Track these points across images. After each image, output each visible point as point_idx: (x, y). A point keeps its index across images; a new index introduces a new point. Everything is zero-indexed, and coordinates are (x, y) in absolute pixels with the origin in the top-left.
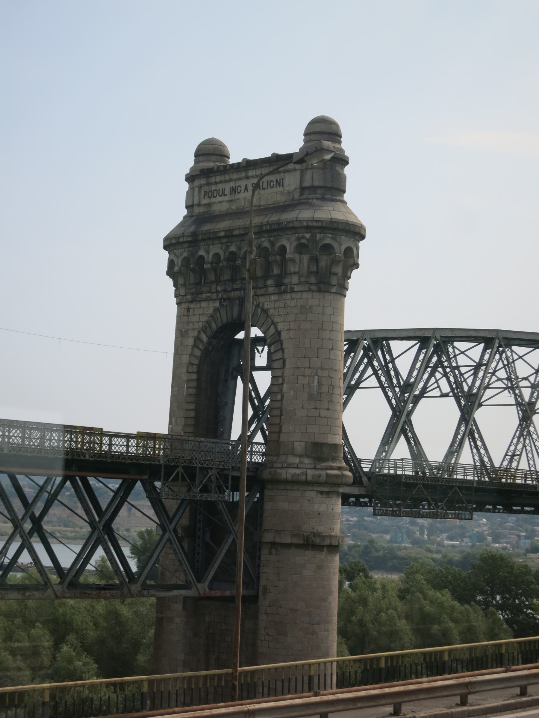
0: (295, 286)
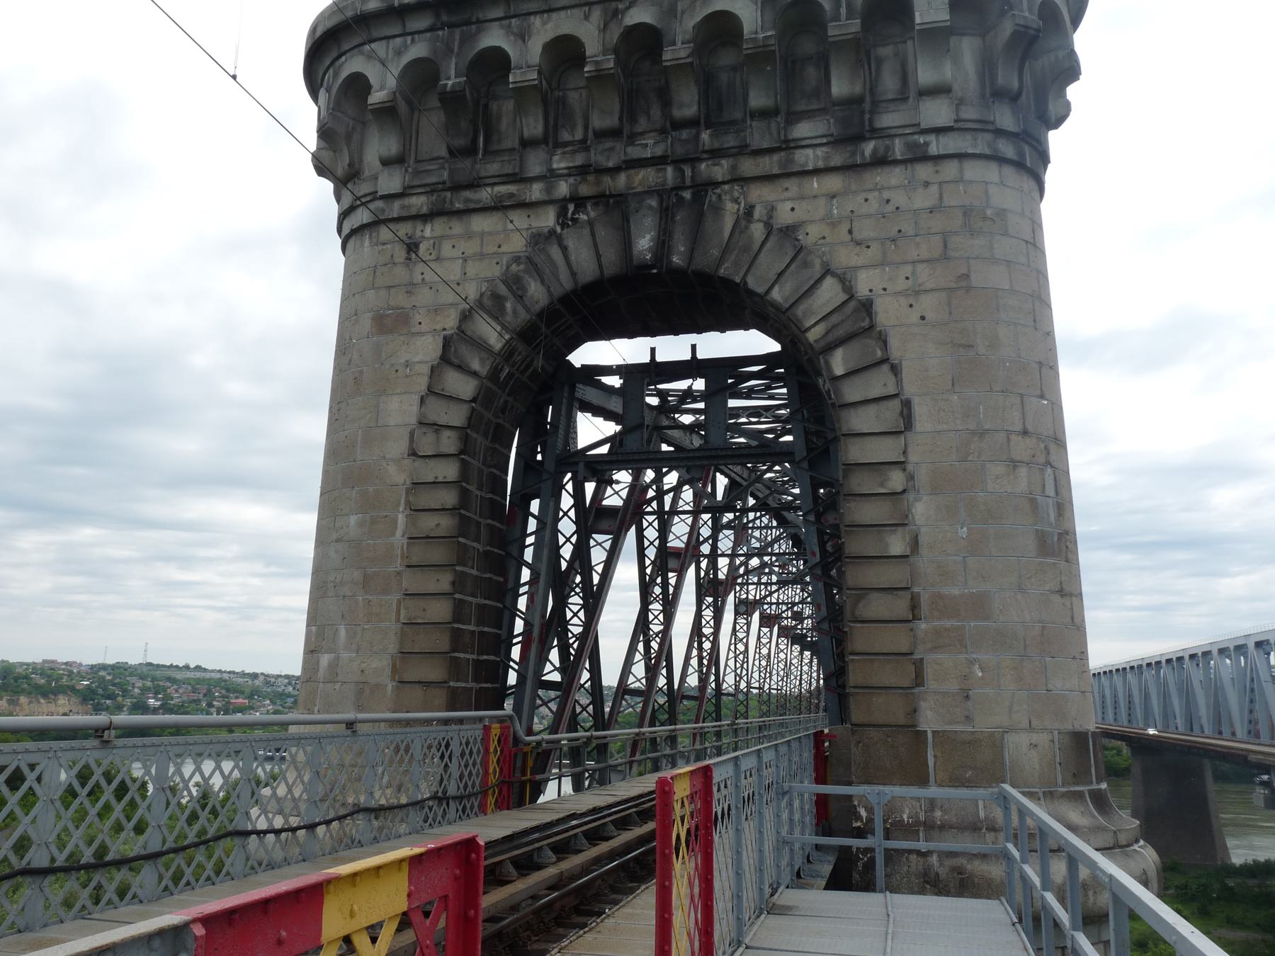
0: (932, 138)
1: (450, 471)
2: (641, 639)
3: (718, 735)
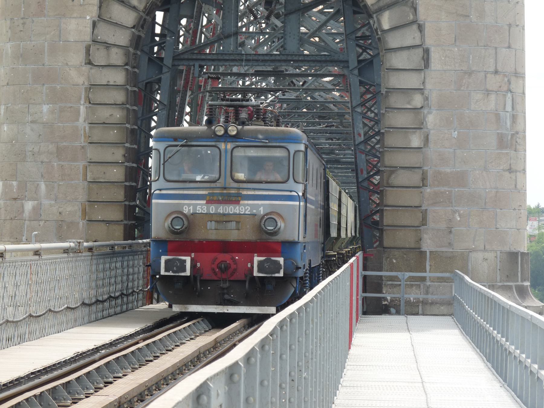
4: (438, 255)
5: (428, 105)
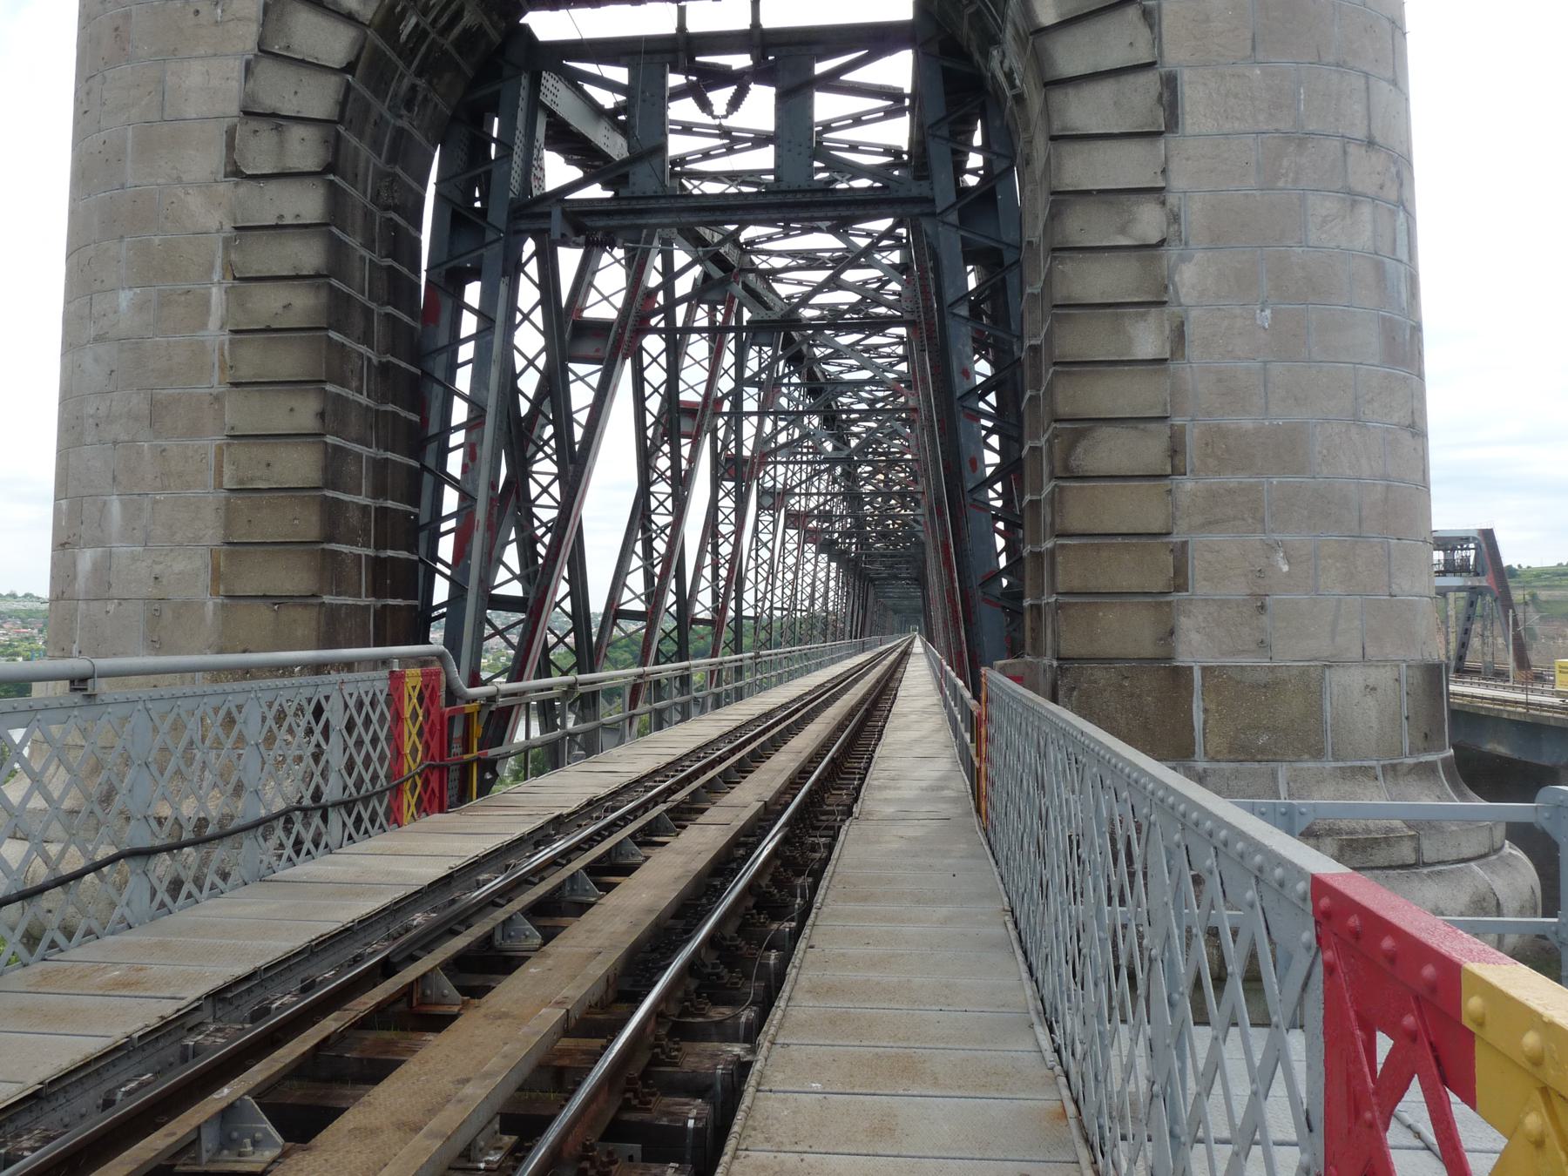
1: (307, 203)
2: (640, 536)
3: (739, 671)
4: (1230, 678)
5: (1180, 235)
